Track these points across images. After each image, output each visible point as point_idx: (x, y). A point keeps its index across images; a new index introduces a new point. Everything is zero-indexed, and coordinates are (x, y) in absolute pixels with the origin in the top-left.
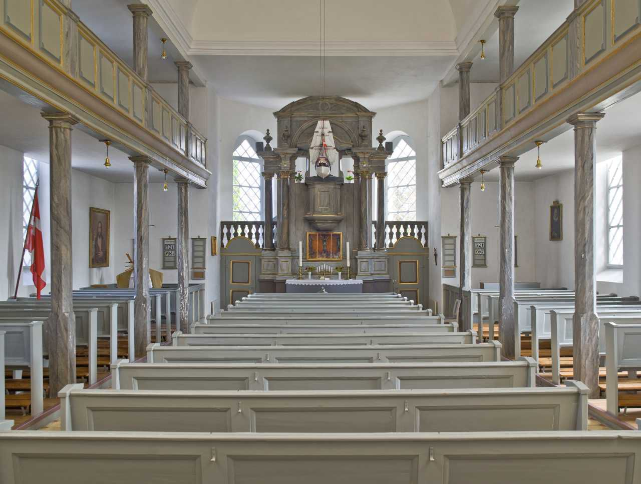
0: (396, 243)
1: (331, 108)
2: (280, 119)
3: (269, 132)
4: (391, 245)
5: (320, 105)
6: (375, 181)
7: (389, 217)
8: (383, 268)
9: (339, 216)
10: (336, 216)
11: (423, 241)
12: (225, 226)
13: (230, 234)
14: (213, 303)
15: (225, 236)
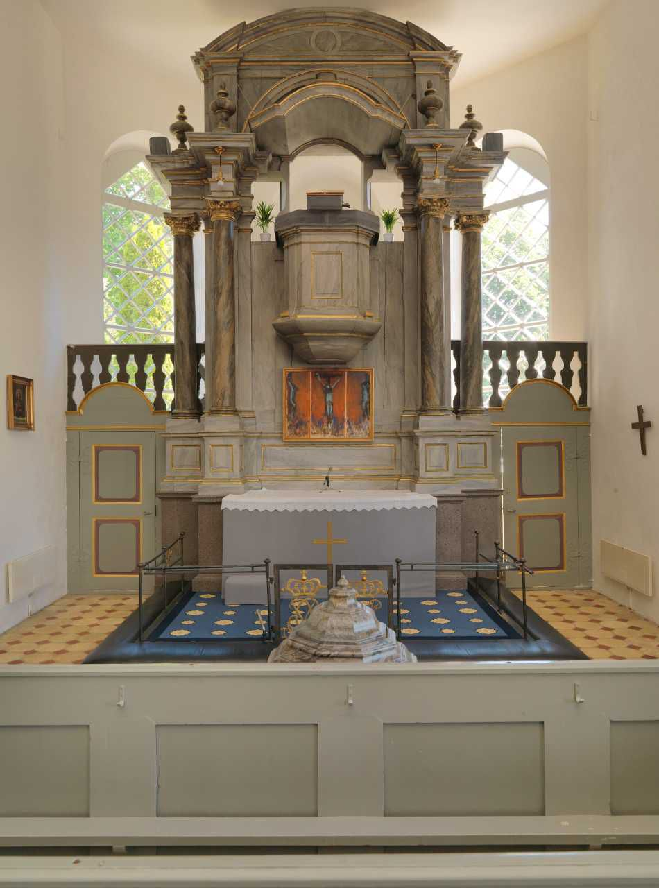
0: (508, 397)
1: (343, 44)
2: (210, 74)
3: (185, 113)
4: (495, 400)
5: (314, 36)
6: (456, 238)
7: (491, 330)
8: (481, 460)
9: (368, 320)
10: (361, 319)
11: (575, 390)
12: (78, 357)
13: (91, 377)
14: (10, 568)
15: (79, 383)
